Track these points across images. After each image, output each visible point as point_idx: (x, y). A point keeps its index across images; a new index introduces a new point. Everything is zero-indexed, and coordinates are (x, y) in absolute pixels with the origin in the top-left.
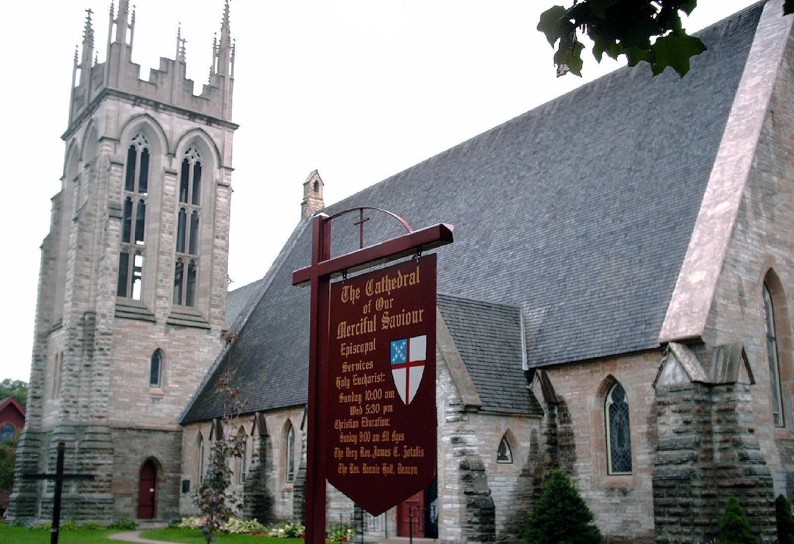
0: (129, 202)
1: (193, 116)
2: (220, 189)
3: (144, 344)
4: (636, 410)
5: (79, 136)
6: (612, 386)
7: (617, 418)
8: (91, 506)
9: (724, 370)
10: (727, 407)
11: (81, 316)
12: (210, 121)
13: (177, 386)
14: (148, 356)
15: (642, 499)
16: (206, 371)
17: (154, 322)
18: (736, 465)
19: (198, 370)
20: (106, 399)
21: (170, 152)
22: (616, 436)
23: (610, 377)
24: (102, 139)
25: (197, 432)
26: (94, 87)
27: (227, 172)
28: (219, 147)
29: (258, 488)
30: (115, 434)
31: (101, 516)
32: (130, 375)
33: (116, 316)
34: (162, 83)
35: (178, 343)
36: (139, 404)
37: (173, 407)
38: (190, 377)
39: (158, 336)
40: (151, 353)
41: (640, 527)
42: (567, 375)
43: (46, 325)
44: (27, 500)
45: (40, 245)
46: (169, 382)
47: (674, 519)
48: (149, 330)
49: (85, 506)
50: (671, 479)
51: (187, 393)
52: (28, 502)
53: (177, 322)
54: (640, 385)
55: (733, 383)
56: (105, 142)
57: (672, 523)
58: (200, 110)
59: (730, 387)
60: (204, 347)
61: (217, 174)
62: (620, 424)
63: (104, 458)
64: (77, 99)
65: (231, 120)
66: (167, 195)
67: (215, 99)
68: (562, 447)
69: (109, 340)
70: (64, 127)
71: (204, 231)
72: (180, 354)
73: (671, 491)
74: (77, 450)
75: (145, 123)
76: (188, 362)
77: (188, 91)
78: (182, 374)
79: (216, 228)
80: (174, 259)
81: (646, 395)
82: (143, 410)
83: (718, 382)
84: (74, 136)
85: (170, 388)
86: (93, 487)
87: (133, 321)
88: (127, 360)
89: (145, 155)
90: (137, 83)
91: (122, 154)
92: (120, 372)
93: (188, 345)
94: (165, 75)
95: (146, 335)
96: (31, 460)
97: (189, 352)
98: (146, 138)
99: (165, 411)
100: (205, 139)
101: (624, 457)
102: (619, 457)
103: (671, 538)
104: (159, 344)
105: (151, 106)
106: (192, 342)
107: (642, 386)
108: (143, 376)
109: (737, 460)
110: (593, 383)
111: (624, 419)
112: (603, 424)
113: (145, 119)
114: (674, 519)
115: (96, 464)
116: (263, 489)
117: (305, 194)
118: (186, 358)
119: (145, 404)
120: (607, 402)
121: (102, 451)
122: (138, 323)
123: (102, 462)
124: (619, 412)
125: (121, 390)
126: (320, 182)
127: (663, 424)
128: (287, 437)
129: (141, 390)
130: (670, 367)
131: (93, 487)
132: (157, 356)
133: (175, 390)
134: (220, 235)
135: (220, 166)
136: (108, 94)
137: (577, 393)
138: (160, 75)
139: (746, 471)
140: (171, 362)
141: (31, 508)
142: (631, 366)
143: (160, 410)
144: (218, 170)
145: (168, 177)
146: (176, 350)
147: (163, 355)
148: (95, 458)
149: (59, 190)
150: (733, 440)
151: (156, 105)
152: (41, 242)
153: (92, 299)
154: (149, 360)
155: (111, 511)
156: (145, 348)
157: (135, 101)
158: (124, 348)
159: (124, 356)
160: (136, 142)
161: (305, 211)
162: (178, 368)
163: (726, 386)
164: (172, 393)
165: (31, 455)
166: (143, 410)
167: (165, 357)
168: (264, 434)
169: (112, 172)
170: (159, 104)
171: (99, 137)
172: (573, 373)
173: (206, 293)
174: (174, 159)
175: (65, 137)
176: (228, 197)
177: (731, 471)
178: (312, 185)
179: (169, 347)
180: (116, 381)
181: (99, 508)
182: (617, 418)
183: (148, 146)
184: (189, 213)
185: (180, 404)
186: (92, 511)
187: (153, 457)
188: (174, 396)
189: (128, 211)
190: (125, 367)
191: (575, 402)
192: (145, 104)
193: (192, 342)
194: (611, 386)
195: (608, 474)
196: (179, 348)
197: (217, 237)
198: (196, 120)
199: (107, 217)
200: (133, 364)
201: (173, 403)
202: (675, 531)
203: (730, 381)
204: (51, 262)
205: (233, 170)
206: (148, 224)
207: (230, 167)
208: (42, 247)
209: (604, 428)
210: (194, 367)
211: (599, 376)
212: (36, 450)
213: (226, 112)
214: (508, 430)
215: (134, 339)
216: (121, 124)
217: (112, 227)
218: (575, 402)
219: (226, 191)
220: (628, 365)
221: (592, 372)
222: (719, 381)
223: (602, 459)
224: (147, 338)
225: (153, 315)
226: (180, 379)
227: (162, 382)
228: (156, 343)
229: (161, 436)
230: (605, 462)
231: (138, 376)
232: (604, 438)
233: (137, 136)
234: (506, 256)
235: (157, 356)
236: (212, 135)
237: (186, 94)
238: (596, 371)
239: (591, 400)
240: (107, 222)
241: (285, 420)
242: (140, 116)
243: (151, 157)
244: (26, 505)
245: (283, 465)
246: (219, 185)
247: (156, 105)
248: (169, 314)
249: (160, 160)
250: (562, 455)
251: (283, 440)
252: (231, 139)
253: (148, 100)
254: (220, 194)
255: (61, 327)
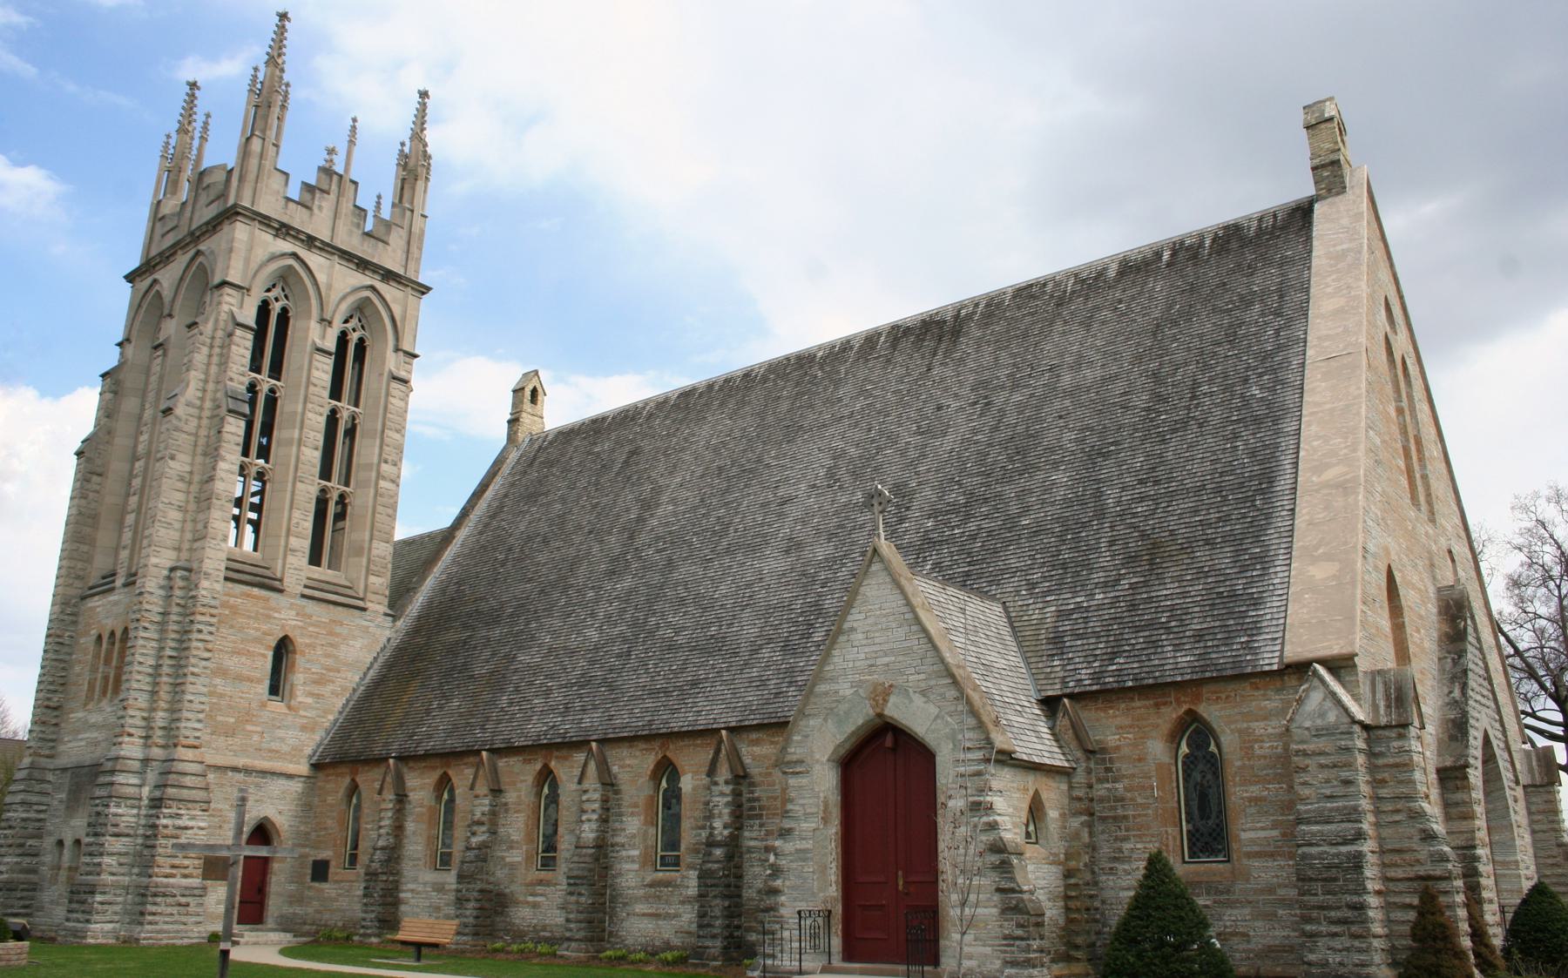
0: (252, 388)
1: (363, 265)
2: (394, 385)
3: (265, 627)
4: (1238, 763)
5: (167, 277)
6: (1195, 731)
7: (1197, 776)
8: (169, 900)
9: (1388, 706)
10: (1398, 760)
11: (166, 573)
12: (389, 276)
13: (310, 700)
14: (268, 647)
15: (1250, 899)
16: (357, 679)
17: (281, 591)
18: (1415, 847)
19: (344, 676)
20: (201, 716)
21: (325, 317)
22: (1195, 804)
23: (1190, 712)
24: (224, 283)
25: (347, 780)
26: (203, 199)
27: (407, 360)
28: (398, 318)
29: (485, 877)
30: (211, 777)
31: (184, 919)
32: (240, 678)
33: (226, 579)
34: (320, 208)
35: (317, 630)
36: (249, 727)
37: (304, 736)
38: (330, 687)
39: (286, 615)
40: (273, 644)
41: (1248, 942)
42: (1111, 708)
43: (78, 583)
44: (22, 886)
45: (75, 450)
46: (298, 693)
47: (1335, 929)
48: (273, 603)
49: (159, 899)
50: (1329, 867)
51: (326, 712)
52: (23, 890)
53: (317, 594)
54: (1245, 725)
55: (1405, 726)
56: (227, 290)
57: (1335, 935)
58: (373, 257)
59: (1401, 730)
60: (354, 638)
61: (392, 362)
62: (1202, 785)
63: (193, 818)
64: (160, 219)
65: (417, 278)
66: (315, 385)
67: (397, 239)
68: (1103, 819)
69: (212, 616)
70: (134, 263)
71: (366, 450)
72: (319, 648)
73: (1333, 886)
74: (145, 802)
75: (290, 267)
76: (330, 662)
77: (358, 226)
78: (318, 682)
79: (385, 447)
80: (314, 491)
81: (1256, 741)
82: (256, 738)
83: (1382, 724)
84: (156, 276)
85: (300, 703)
86: (173, 867)
87: (249, 588)
88: (236, 652)
89: (284, 317)
90: (283, 201)
91: (249, 316)
92: (222, 672)
93: (331, 633)
94: (326, 195)
95: (266, 612)
96: (33, 815)
97: (332, 645)
98: (287, 291)
99: (291, 742)
100: (314, 302)
101: (1210, 835)
102: (1202, 835)
103: (1334, 959)
104: (287, 628)
105: (303, 241)
106: (338, 629)
107: (1249, 728)
108: (259, 681)
109: (1416, 838)
110: (1160, 721)
111: (1209, 776)
112: (1175, 784)
113: (291, 262)
114: (1335, 929)
115: (180, 828)
116: (492, 879)
117: (514, 405)
118: (327, 656)
119: (259, 729)
120: (1180, 752)
121: (190, 805)
122: (256, 591)
123: (191, 823)
124: (1201, 767)
125: (222, 703)
126: (540, 390)
127: (1305, 784)
128: (439, 798)
129: (254, 705)
130: (1315, 698)
131: (173, 867)
132: (283, 649)
133: (308, 707)
134: (390, 458)
135: (397, 349)
136: (238, 214)
137: (1130, 736)
138: (318, 194)
139: (1432, 856)
140: (303, 659)
141: (27, 902)
142: (1227, 697)
143: (282, 740)
144: (394, 354)
145: (318, 357)
146: (313, 640)
147: (291, 648)
148: (179, 816)
149: (115, 363)
150: (1410, 810)
151: (310, 242)
152: (77, 445)
153: (186, 546)
154: (270, 654)
155: (199, 910)
156: (265, 633)
157: (277, 230)
158: (231, 631)
159: (231, 645)
160: (271, 295)
161: (516, 432)
162: (313, 670)
163: (1395, 730)
164: (302, 713)
165: (35, 807)
166: (256, 738)
167: (294, 652)
168: (401, 793)
169: (235, 339)
170: (315, 239)
171: (217, 280)
172: (1123, 706)
173: (358, 551)
174: (329, 329)
175: (131, 278)
176: (405, 399)
177: (1407, 856)
178: (528, 393)
179: (302, 635)
180: (216, 686)
181: (180, 905)
182: (1197, 776)
183: (290, 304)
184: (344, 416)
185: (313, 730)
186: (169, 910)
187: (266, 818)
188: (305, 717)
189: (252, 403)
190: (232, 663)
191: (1126, 751)
192: (294, 237)
193: (338, 629)
194: (1188, 728)
195: (1184, 862)
196: (316, 638)
197: (386, 462)
198: (367, 272)
199: (223, 411)
200: (243, 659)
201: (304, 728)
202: (1340, 947)
203: (1402, 721)
204: (95, 479)
205: (416, 356)
206: (280, 429)
207: (411, 351)
208: (79, 454)
209: (1175, 790)
210: (339, 672)
211: (1171, 714)
212: (44, 799)
213: (411, 265)
214: (1036, 790)
215: (249, 617)
216: (254, 266)
217: (227, 428)
218: (1126, 751)
219: (403, 388)
220: (1223, 696)
221: (1157, 706)
222: (1383, 721)
223: (1174, 838)
224: (269, 617)
225: (281, 580)
226: (316, 689)
227: (287, 693)
228: (283, 626)
229: (282, 782)
230: (1178, 842)
231: (250, 680)
232: (1176, 805)
233: (274, 286)
234: (946, 523)
235: (283, 649)
236: (388, 297)
237: (355, 230)
238: (1165, 704)
239: (1157, 749)
240: (223, 419)
241: (538, 766)
242: (283, 255)
243: (291, 322)
244: (19, 895)
245: (532, 841)
246: (395, 378)
247: (310, 242)
248: (306, 582)
249: (308, 328)
250: (1103, 832)
251: (532, 799)
252: (418, 310)
253: (299, 231)
254: (394, 392)
255: (113, 589)
